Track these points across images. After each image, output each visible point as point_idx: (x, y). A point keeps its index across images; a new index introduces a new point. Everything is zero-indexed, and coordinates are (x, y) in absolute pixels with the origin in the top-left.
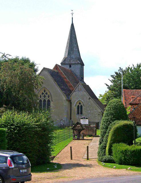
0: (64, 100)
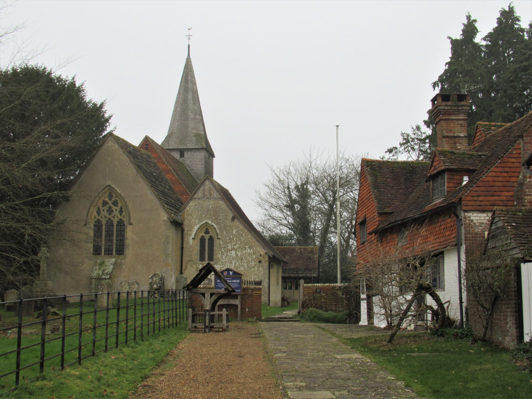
0: (164, 221)
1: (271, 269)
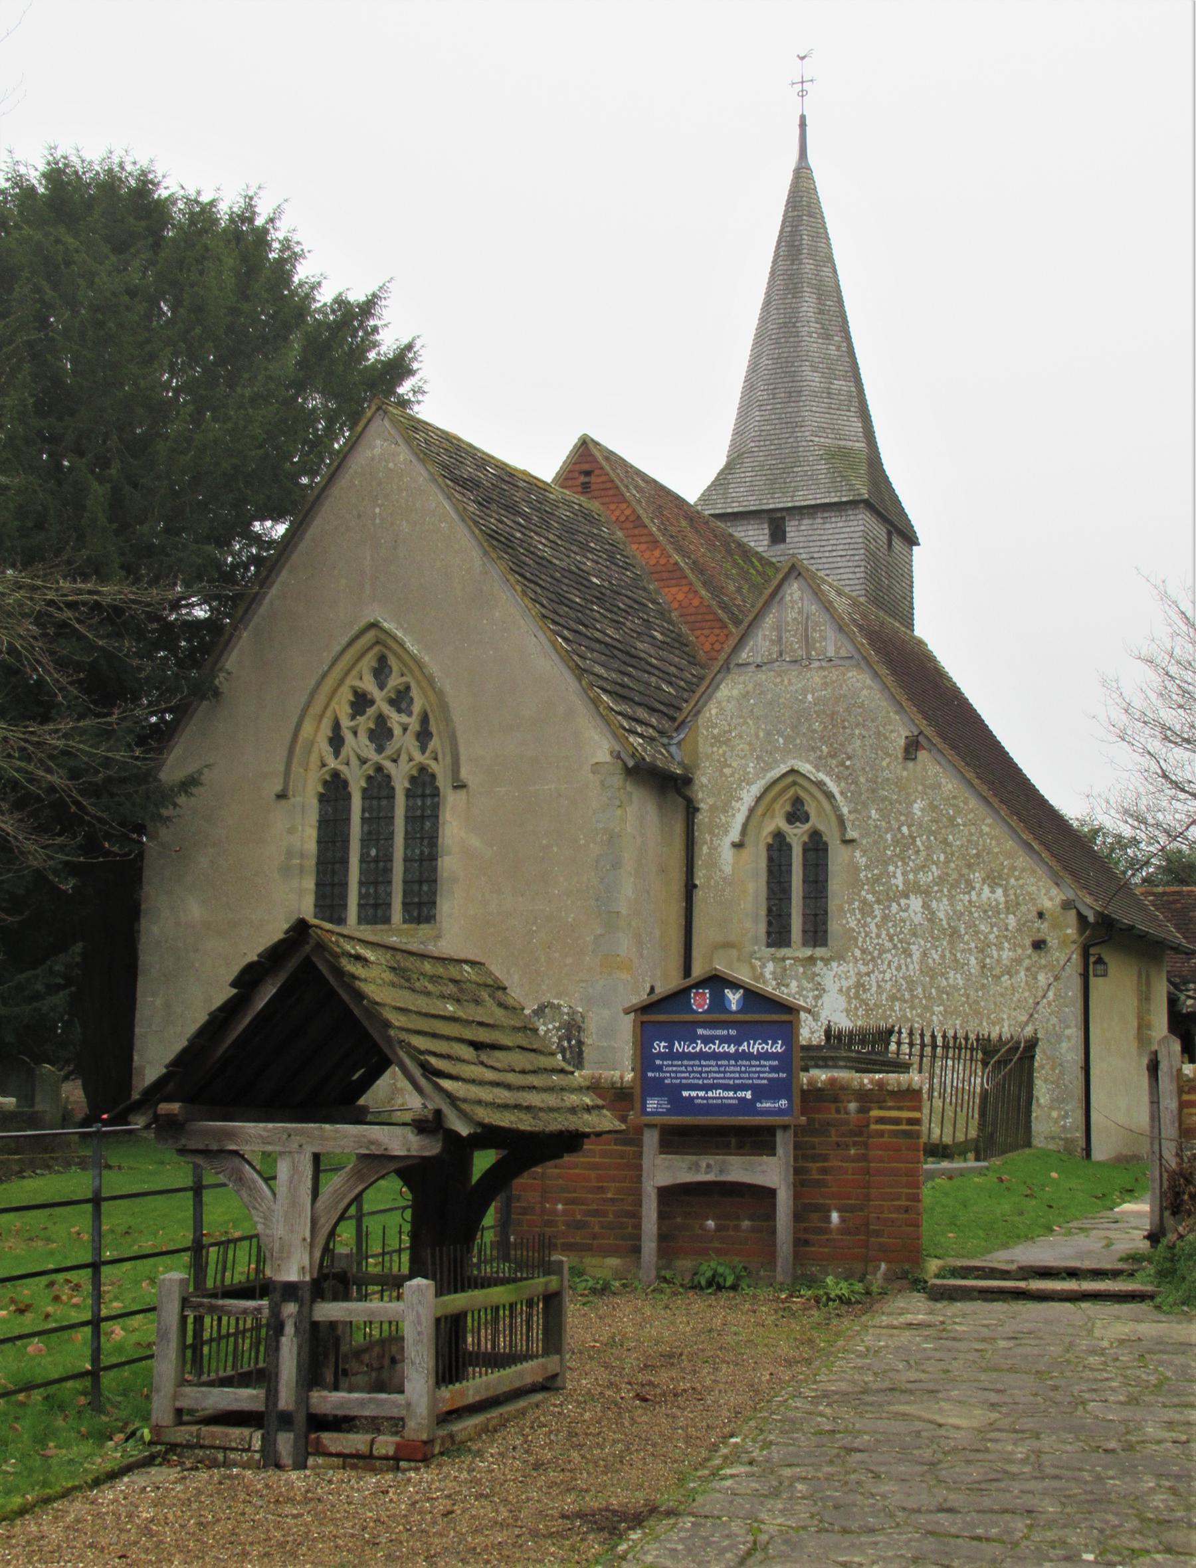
1: (1093, 980)
